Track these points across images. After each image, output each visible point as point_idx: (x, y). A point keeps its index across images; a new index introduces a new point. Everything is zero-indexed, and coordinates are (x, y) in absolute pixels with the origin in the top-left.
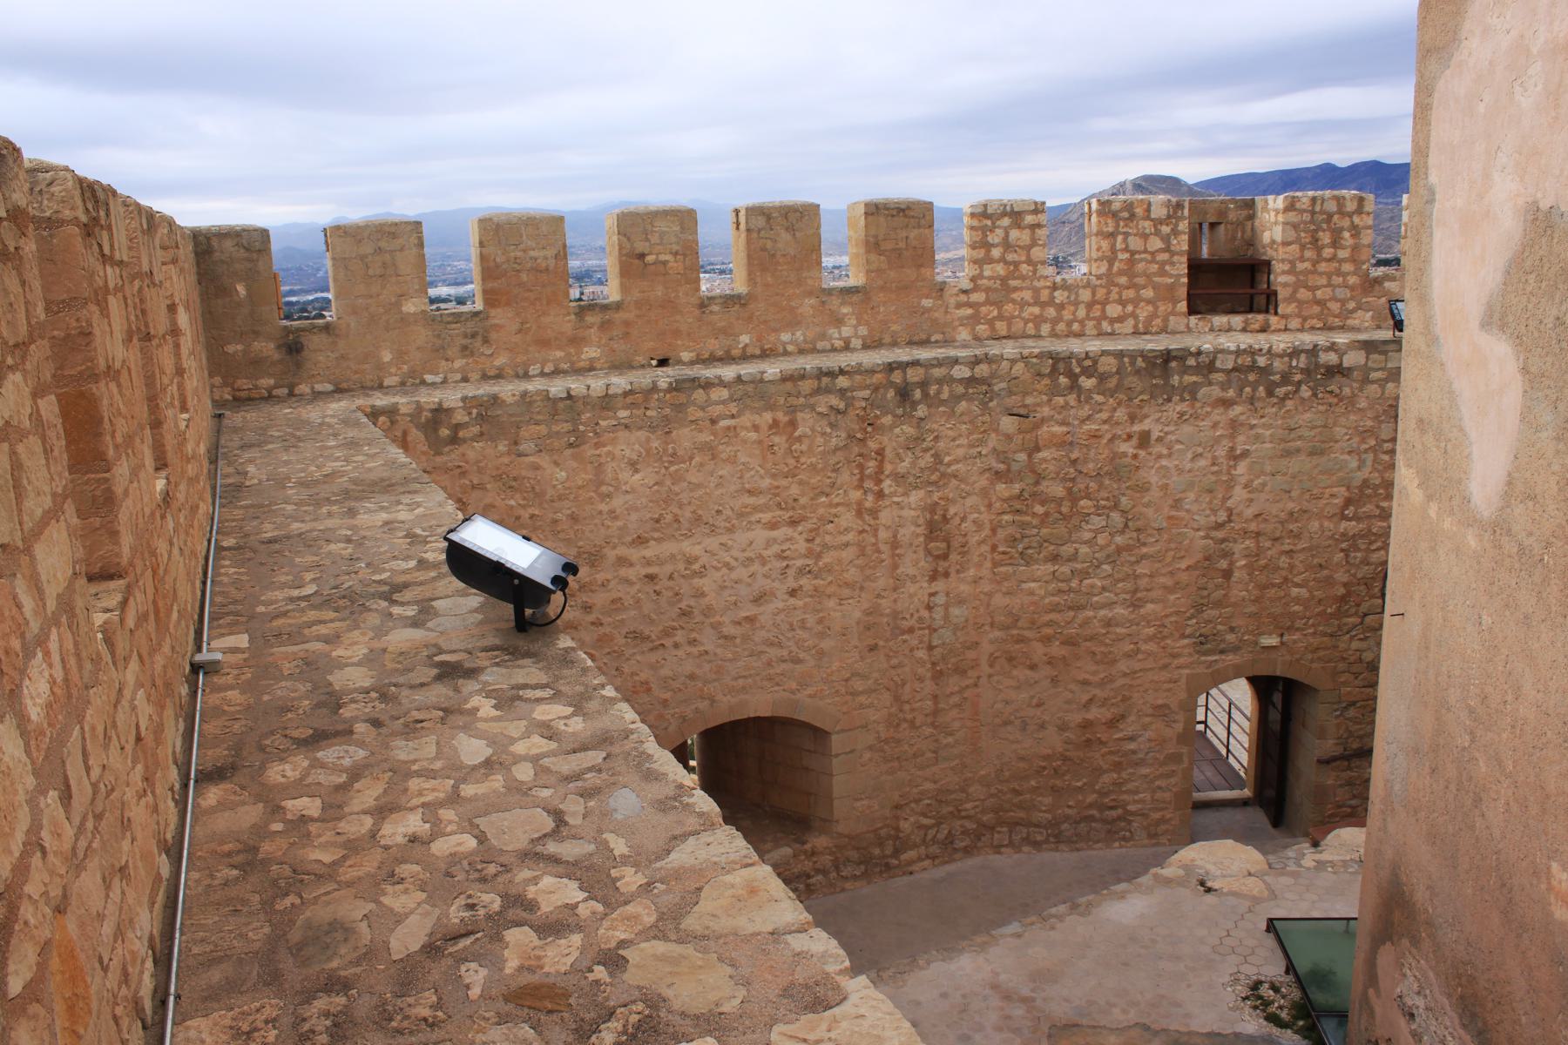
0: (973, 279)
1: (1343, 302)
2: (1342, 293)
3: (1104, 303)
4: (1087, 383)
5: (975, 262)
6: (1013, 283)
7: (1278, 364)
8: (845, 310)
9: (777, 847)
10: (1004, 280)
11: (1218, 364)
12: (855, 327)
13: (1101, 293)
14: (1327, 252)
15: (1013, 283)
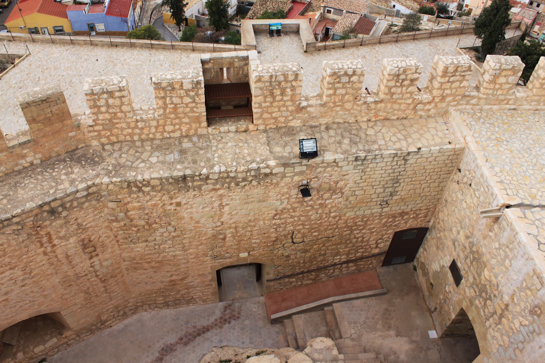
0: (94, 121)
1: (286, 117)
2: (284, 114)
3: (164, 126)
4: (147, 189)
5: (93, 114)
6: (115, 121)
7: (240, 175)
8: (25, 151)
9: (51, 338)
10: (110, 120)
11: (210, 177)
12: (34, 156)
13: (161, 122)
14: (279, 98)
15: (115, 121)
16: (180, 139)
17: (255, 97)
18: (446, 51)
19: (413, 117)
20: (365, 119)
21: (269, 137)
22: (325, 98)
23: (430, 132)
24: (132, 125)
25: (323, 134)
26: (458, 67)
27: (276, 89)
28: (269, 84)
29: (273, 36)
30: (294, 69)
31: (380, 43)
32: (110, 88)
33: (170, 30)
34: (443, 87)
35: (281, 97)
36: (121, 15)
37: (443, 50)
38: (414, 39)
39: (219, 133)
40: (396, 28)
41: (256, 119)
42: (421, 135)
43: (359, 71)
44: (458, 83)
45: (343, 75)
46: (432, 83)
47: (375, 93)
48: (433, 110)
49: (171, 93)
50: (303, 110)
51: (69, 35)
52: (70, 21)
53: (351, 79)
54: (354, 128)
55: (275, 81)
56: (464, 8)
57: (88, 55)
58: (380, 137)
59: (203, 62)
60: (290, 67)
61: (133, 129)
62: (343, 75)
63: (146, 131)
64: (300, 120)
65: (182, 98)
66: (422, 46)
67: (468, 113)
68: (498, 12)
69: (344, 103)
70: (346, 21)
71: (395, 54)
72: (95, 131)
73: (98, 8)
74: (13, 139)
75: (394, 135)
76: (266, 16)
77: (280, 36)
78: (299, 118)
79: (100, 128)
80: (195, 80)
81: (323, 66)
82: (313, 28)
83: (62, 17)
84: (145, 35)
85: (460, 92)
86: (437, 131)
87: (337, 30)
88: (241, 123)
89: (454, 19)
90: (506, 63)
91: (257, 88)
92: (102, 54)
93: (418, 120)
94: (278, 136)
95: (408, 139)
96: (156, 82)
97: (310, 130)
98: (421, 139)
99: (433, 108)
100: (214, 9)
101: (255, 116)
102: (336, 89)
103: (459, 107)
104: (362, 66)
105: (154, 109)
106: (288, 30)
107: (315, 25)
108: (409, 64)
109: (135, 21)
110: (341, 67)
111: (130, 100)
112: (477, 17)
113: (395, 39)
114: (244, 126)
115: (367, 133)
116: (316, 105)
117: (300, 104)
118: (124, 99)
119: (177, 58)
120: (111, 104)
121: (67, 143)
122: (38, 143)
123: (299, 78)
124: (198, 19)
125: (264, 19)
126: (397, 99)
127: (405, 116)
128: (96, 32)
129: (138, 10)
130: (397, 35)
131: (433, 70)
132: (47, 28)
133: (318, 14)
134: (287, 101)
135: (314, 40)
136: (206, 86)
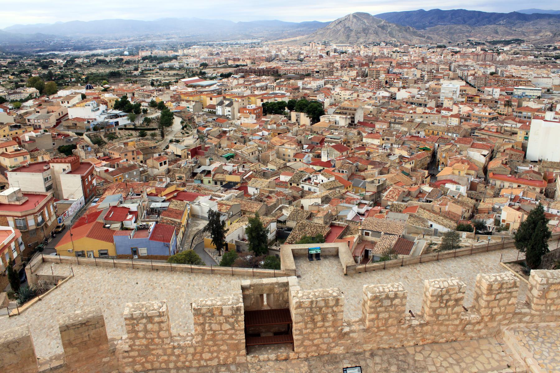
0: (130, 346)
1: (328, 344)
3: (201, 353)
5: (130, 339)
6: (151, 347)
10: (147, 346)
13: (199, 349)
14: (319, 324)
15: (151, 347)
16: (217, 368)
17: (296, 323)
18: (490, 267)
19: (463, 339)
20: (412, 343)
21: (311, 366)
22: (367, 323)
23: (484, 354)
24: (169, 351)
25: (368, 361)
26: (503, 284)
27: (317, 315)
28: (309, 309)
29: (312, 260)
30: (335, 294)
31: (421, 262)
32: (150, 313)
33: (210, 254)
34: (490, 306)
35: (322, 323)
36: (164, 241)
37: (487, 266)
38: (455, 257)
39: (258, 361)
40: (435, 247)
41: (297, 346)
42: (475, 358)
43: (400, 294)
44: (506, 301)
45: (385, 299)
46: (478, 302)
47: (419, 316)
48: (483, 330)
49: (210, 319)
50: (346, 336)
51: (113, 258)
52: (115, 246)
53: (394, 302)
54: (401, 353)
55: (316, 307)
56: (502, 223)
57: (128, 278)
58: (430, 363)
59: (243, 289)
60: (331, 292)
61: (169, 355)
62: (385, 299)
63: (182, 359)
64: (343, 347)
65: (221, 324)
66: (464, 263)
67: (524, 332)
68: (535, 226)
69: (388, 327)
70: (385, 243)
71: (437, 273)
72: (130, 357)
73: (143, 233)
74: (46, 363)
75: (445, 359)
76: (305, 240)
77: (319, 259)
78: (342, 345)
79: (136, 354)
80: (235, 306)
81: (364, 290)
82: (352, 251)
83: (108, 241)
84: (185, 259)
85: (510, 309)
86: (492, 353)
87: (377, 251)
88: (281, 350)
89: (494, 234)
90: (553, 277)
91: (297, 314)
92: (142, 277)
93: (469, 341)
94: (320, 364)
95: (461, 364)
96: (196, 308)
97: (354, 357)
98: (476, 363)
99: (484, 328)
100: (254, 234)
101: (296, 343)
102: (378, 313)
103: (512, 326)
104: (403, 288)
105: (192, 335)
106: (327, 253)
107: (354, 247)
108: (452, 284)
109: (176, 246)
110: (382, 290)
111: (168, 325)
112: (516, 231)
113: (436, 258)
114: (285, 354)
115: (416, 358)
116: (359, 331)
117: (342, 329)
118: (162, 325)
119: (217, 282)
120: (150, 330)
121: (99, 369)
122: (70, 368)
123: (340, 304)
124: (238, 244)
125: (302, 243)
126: (443, 320)
127: (454, 338)
128: (139, 256)
129: (180, 235)
130: (437, 254)
131: (477, 289)
132: (92, 251)
133: (356, 237)
134: (329, 327)
135: (354, 262)
136: (245, 313)
